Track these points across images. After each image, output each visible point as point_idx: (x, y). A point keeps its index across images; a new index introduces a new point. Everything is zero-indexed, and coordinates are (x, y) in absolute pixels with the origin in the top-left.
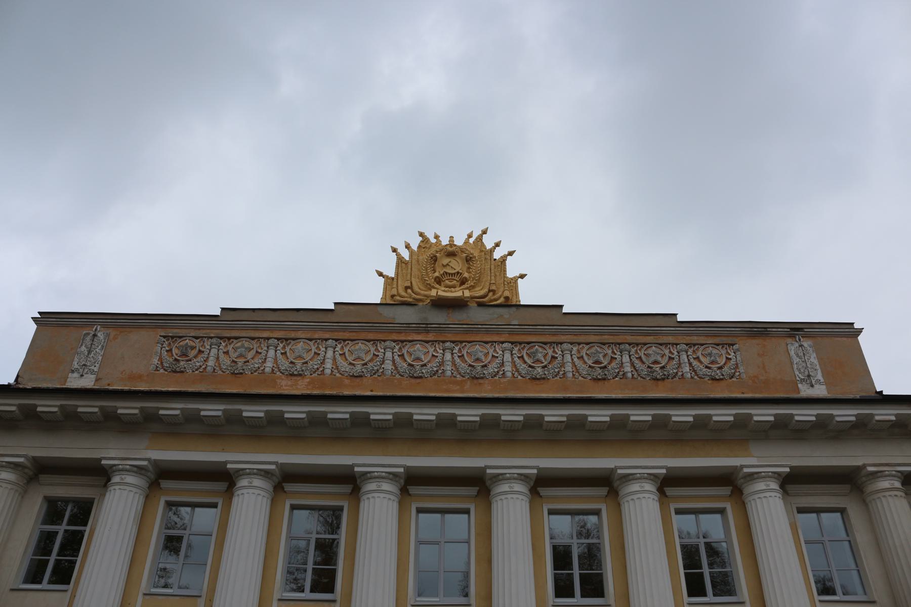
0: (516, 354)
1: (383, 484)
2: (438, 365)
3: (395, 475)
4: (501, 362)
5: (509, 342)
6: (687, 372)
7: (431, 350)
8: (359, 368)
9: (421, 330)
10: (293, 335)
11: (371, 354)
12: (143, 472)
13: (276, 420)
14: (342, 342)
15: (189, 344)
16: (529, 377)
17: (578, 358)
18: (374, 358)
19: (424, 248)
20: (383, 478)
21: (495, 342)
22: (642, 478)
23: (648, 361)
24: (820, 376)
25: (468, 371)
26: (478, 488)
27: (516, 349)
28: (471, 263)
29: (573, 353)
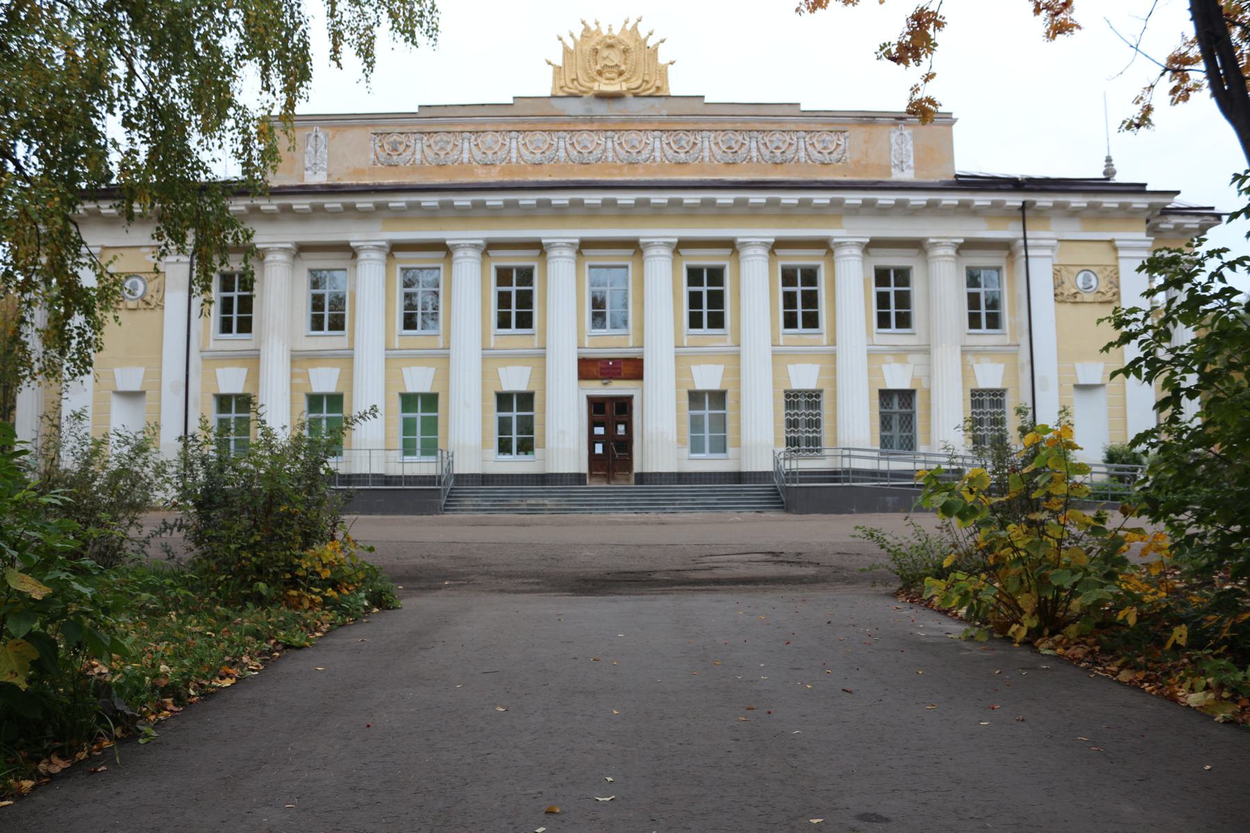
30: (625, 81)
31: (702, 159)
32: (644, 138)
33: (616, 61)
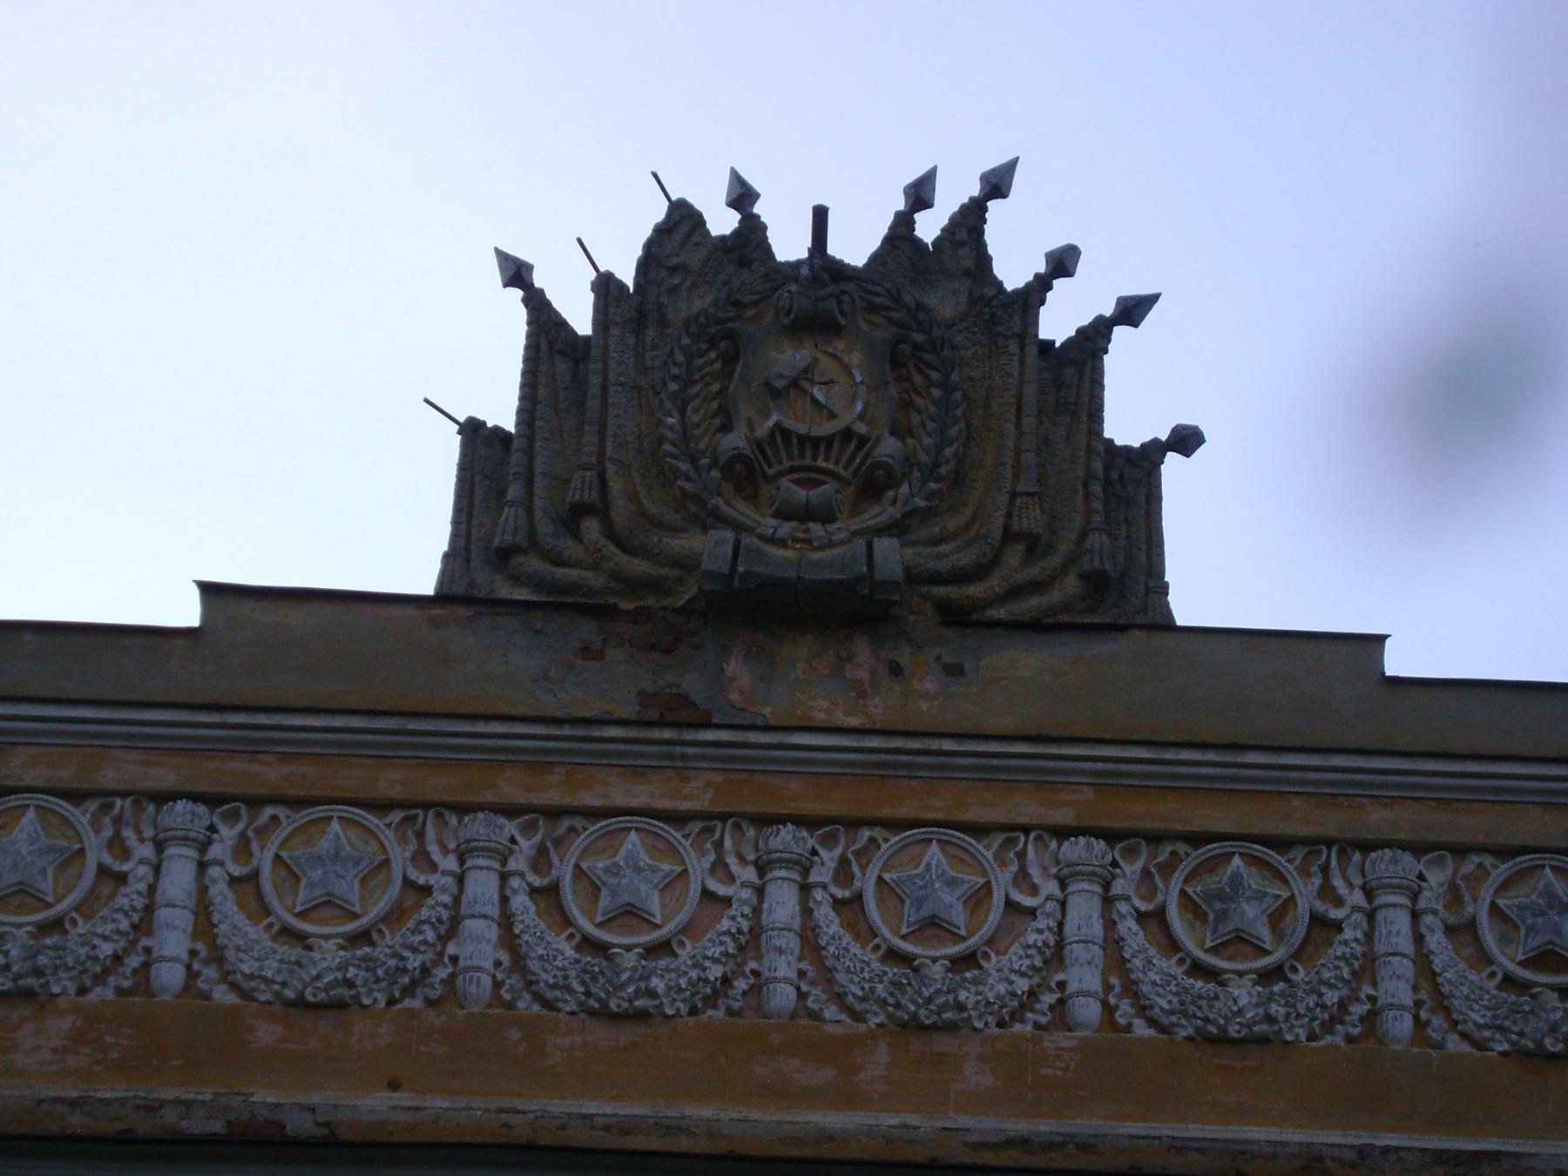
0: (1127, 899)
2: (1038, 962)
4: (1052, 940)
5: (1098, 833)
8: (328, 956)
9: (651, 756)
11: (389, 880)
14: (244, 811)
16: (1190, 1031)
17: (1450, 930)
18: (409, 903)
19: (673, 270)
21: (1026, 830)
25: (880, 987)
27: (1133, 868)
28: (918, 380)
29: (1422, 904)
30: (895, 529)
31: (1371, 1018)
32: (1002, 880)
33: (849, 415)
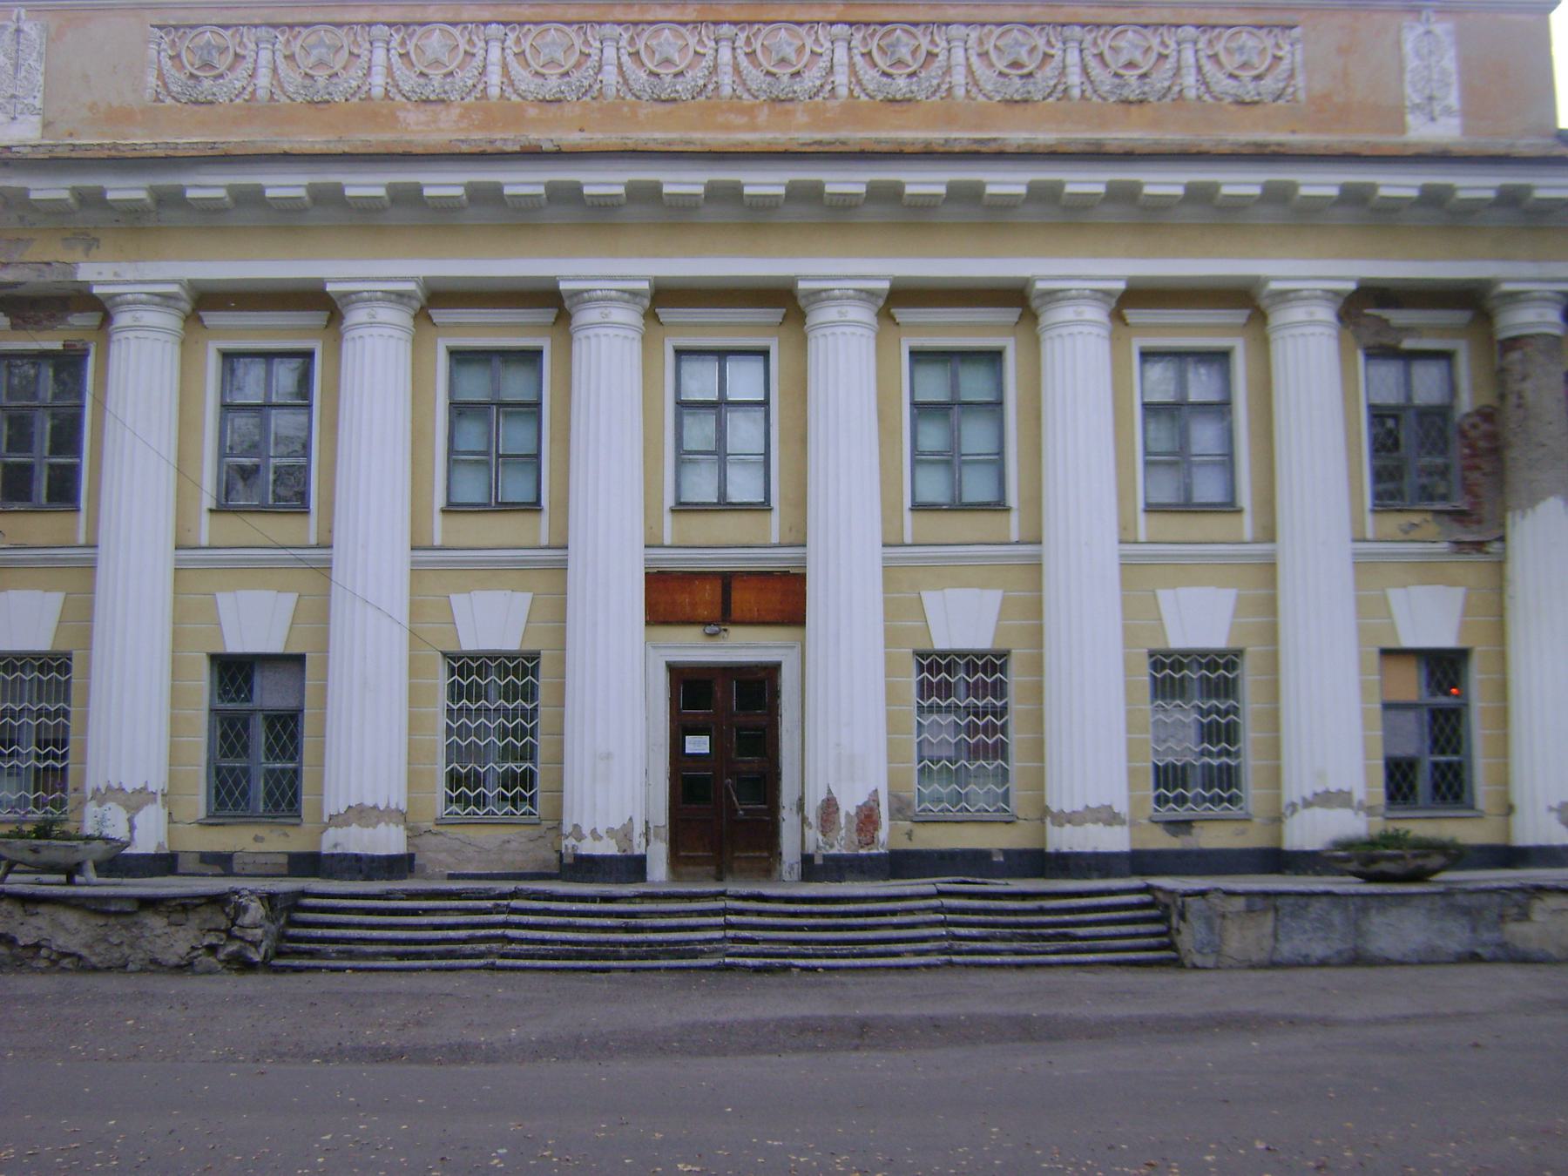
1: (613, 311)
3: (634, 294)
4: (829, 65)
5: (845, 23)
6: (1189, 87)
7: (692, 41)
10: (419, 15)
12: (172, 303)
13: (407, 197)
14: (517, 27)
15: (213, 42)
18: (582, 61)
20: (611, 300)
22: (1080, 297)
23: (1115, 63)
24: (1453, 99)
26: (784, 310)
